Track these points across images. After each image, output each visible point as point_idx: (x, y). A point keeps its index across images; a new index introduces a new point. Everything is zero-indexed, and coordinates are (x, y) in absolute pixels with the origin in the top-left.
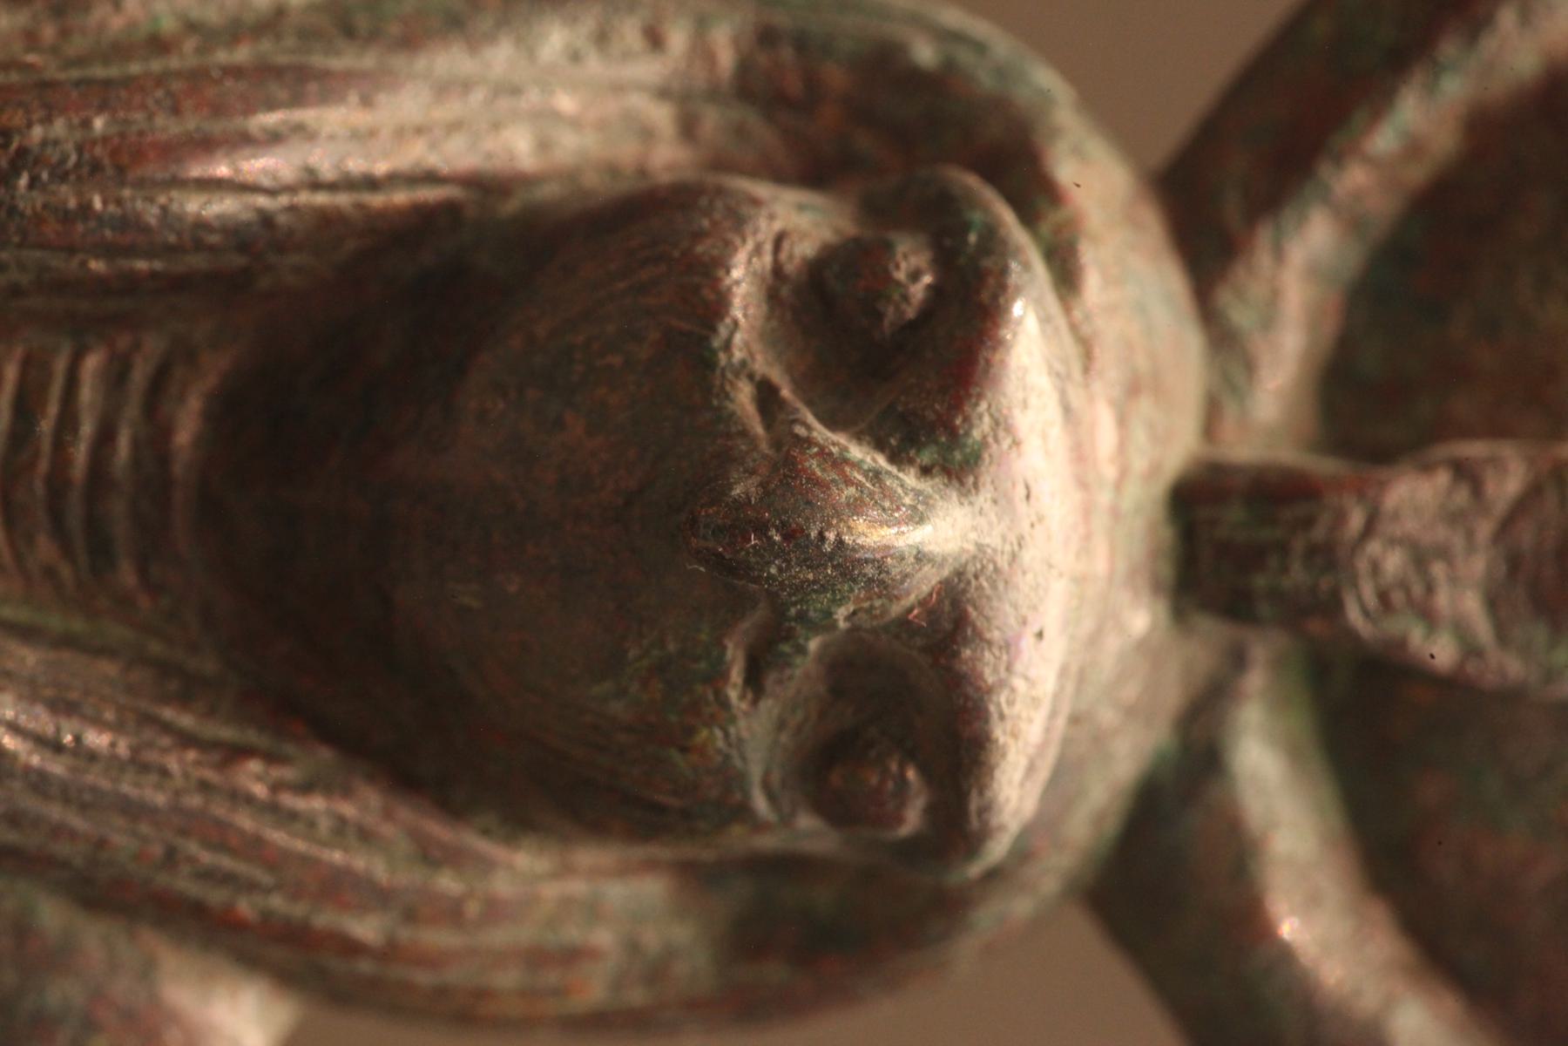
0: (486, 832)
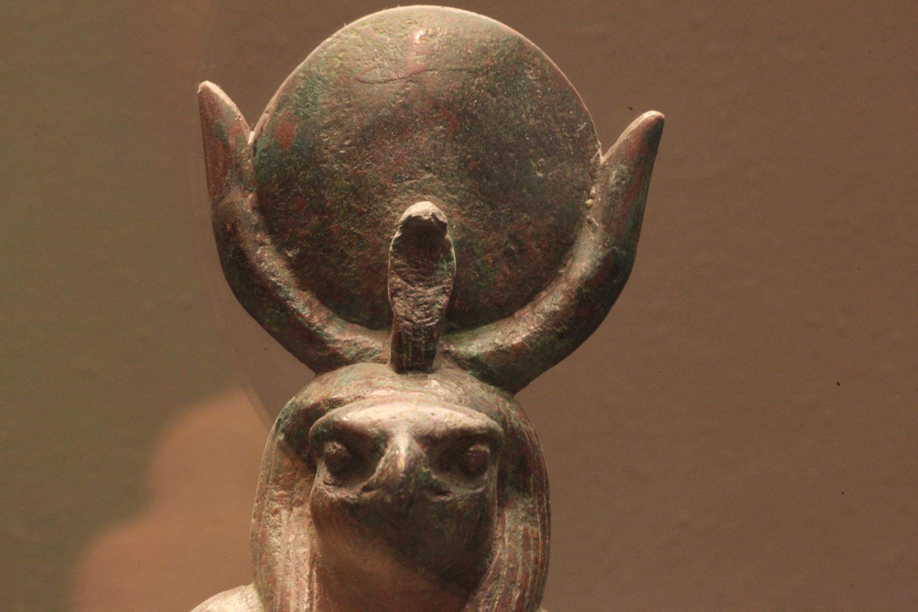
0: (491, 562)
